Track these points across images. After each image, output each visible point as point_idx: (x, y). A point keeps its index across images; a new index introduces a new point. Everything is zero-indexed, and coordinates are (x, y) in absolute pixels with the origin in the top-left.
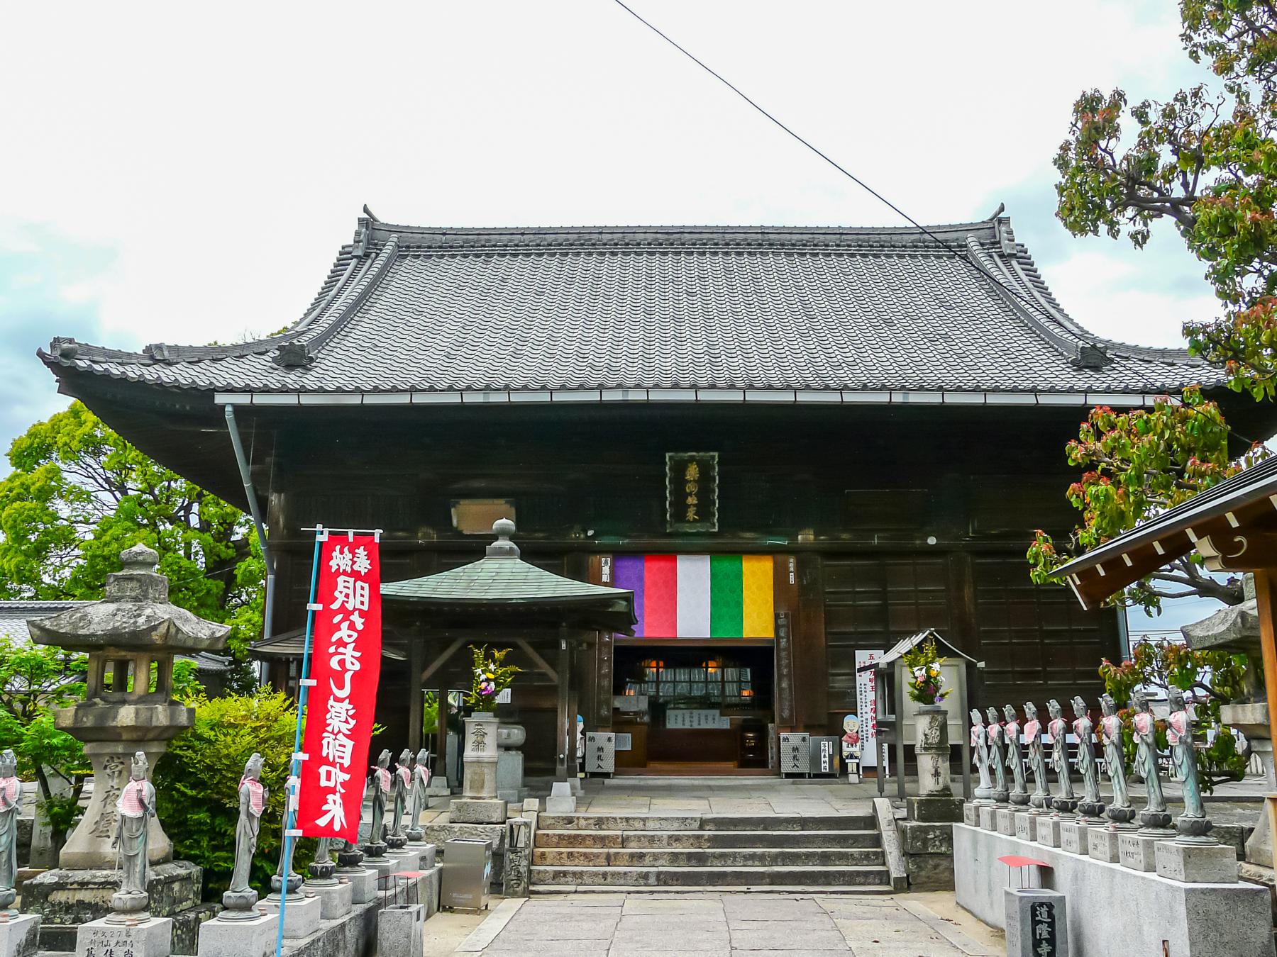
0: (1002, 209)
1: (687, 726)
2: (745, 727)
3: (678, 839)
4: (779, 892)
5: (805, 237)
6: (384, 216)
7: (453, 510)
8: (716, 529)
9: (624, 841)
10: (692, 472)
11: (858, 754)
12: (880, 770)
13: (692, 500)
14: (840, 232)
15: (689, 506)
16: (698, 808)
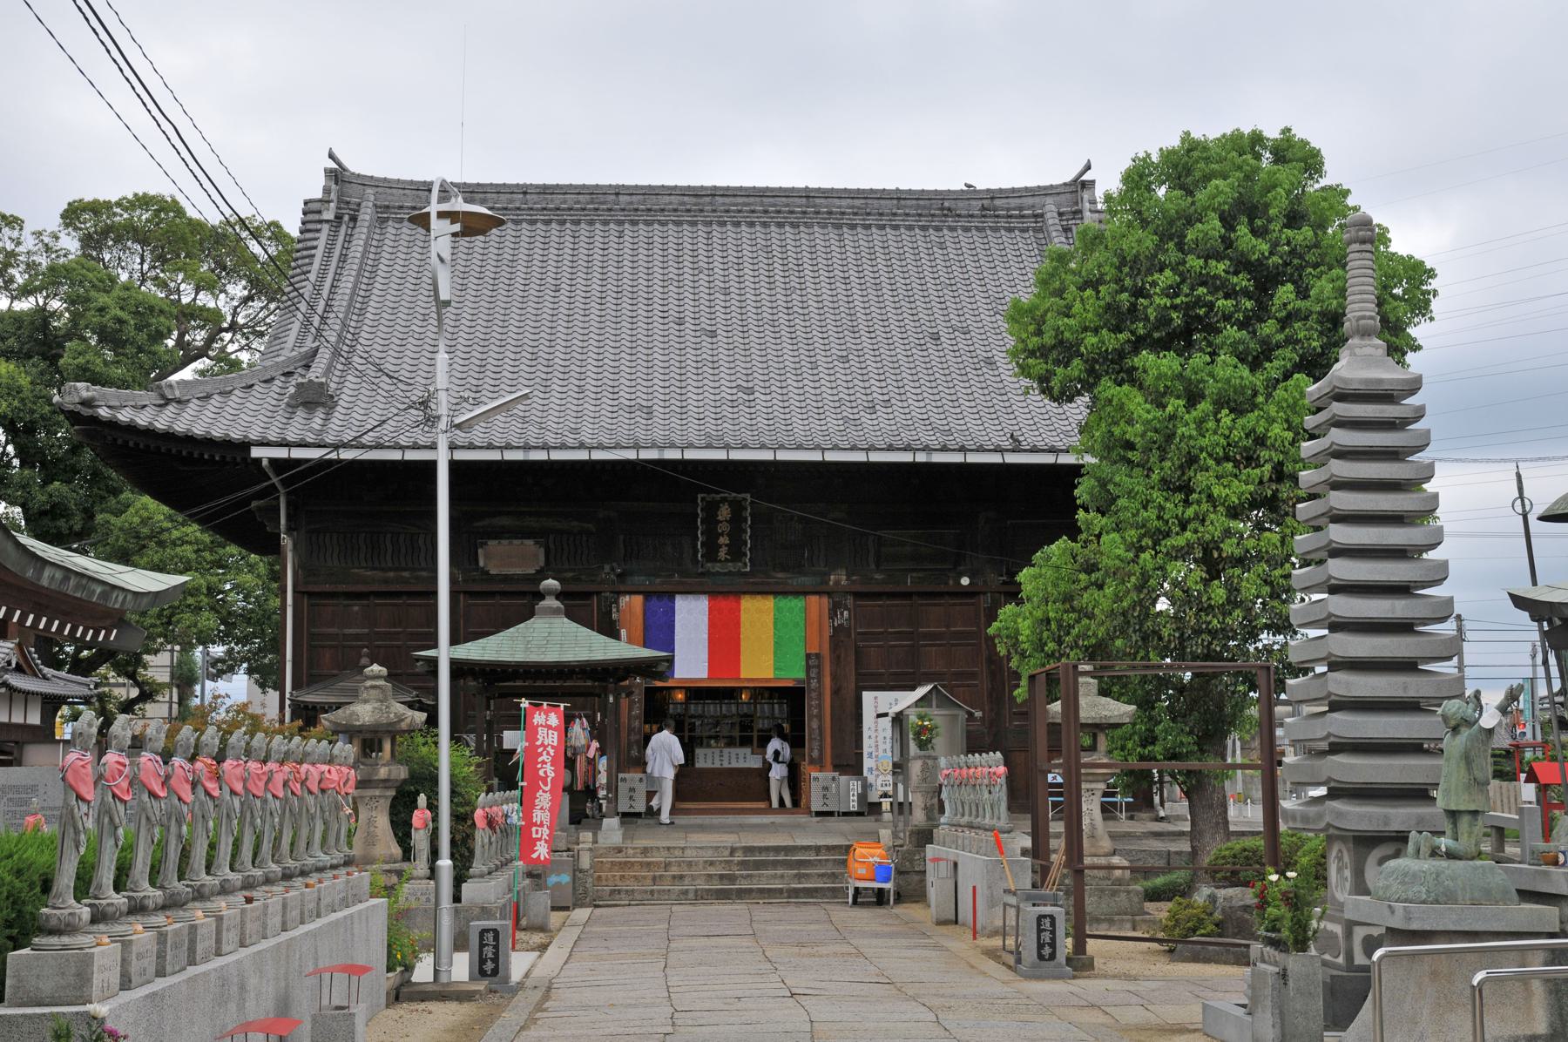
0: (1088, 167)
1: (717, 765)
3: (712, 863)
5: (857, 202)
6: (357, 164)
9: (667, 866)
10: (724, 512)
13: (723, 540)
14: (898, 196)
16: (729, 839)
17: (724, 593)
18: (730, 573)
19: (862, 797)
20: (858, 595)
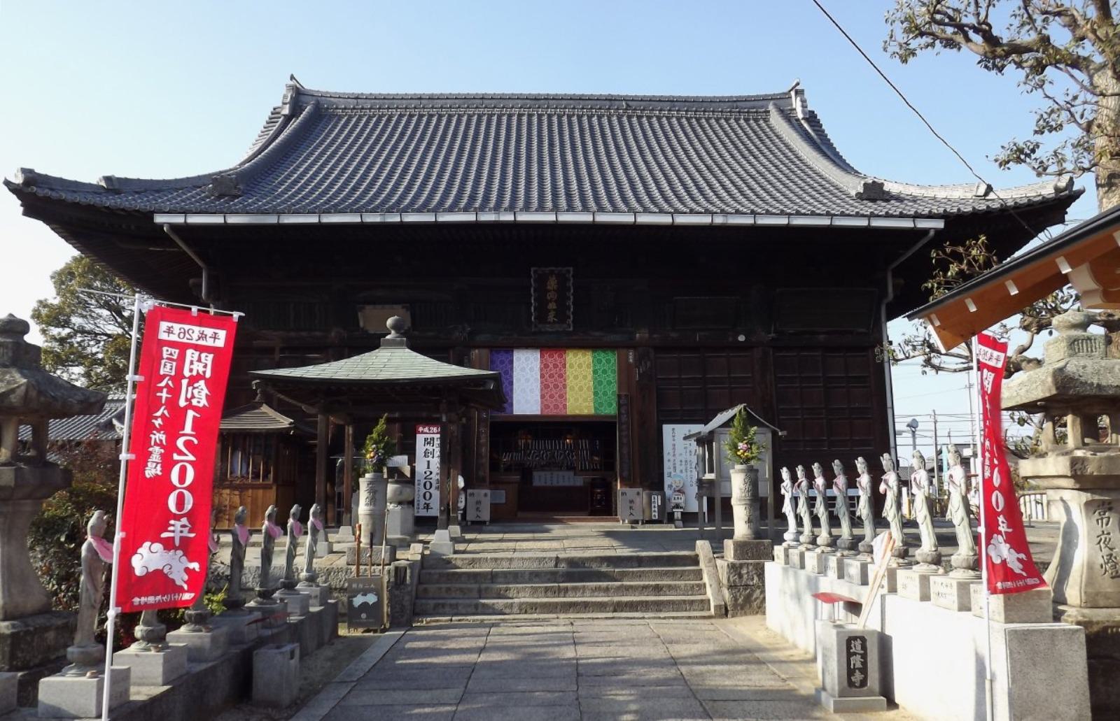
2: (593, 484)
4: (620, 618)
6: (309, 84)
7: (359, 314)
8: (571, 329)
10: (552, 283)
11: (683, 505)
12: (700, 517)
13: (552, 306)
15: (549, 311)
17: (551, 344)
18: (557, 332)
19: (662, 508)
20: (658, 349)
